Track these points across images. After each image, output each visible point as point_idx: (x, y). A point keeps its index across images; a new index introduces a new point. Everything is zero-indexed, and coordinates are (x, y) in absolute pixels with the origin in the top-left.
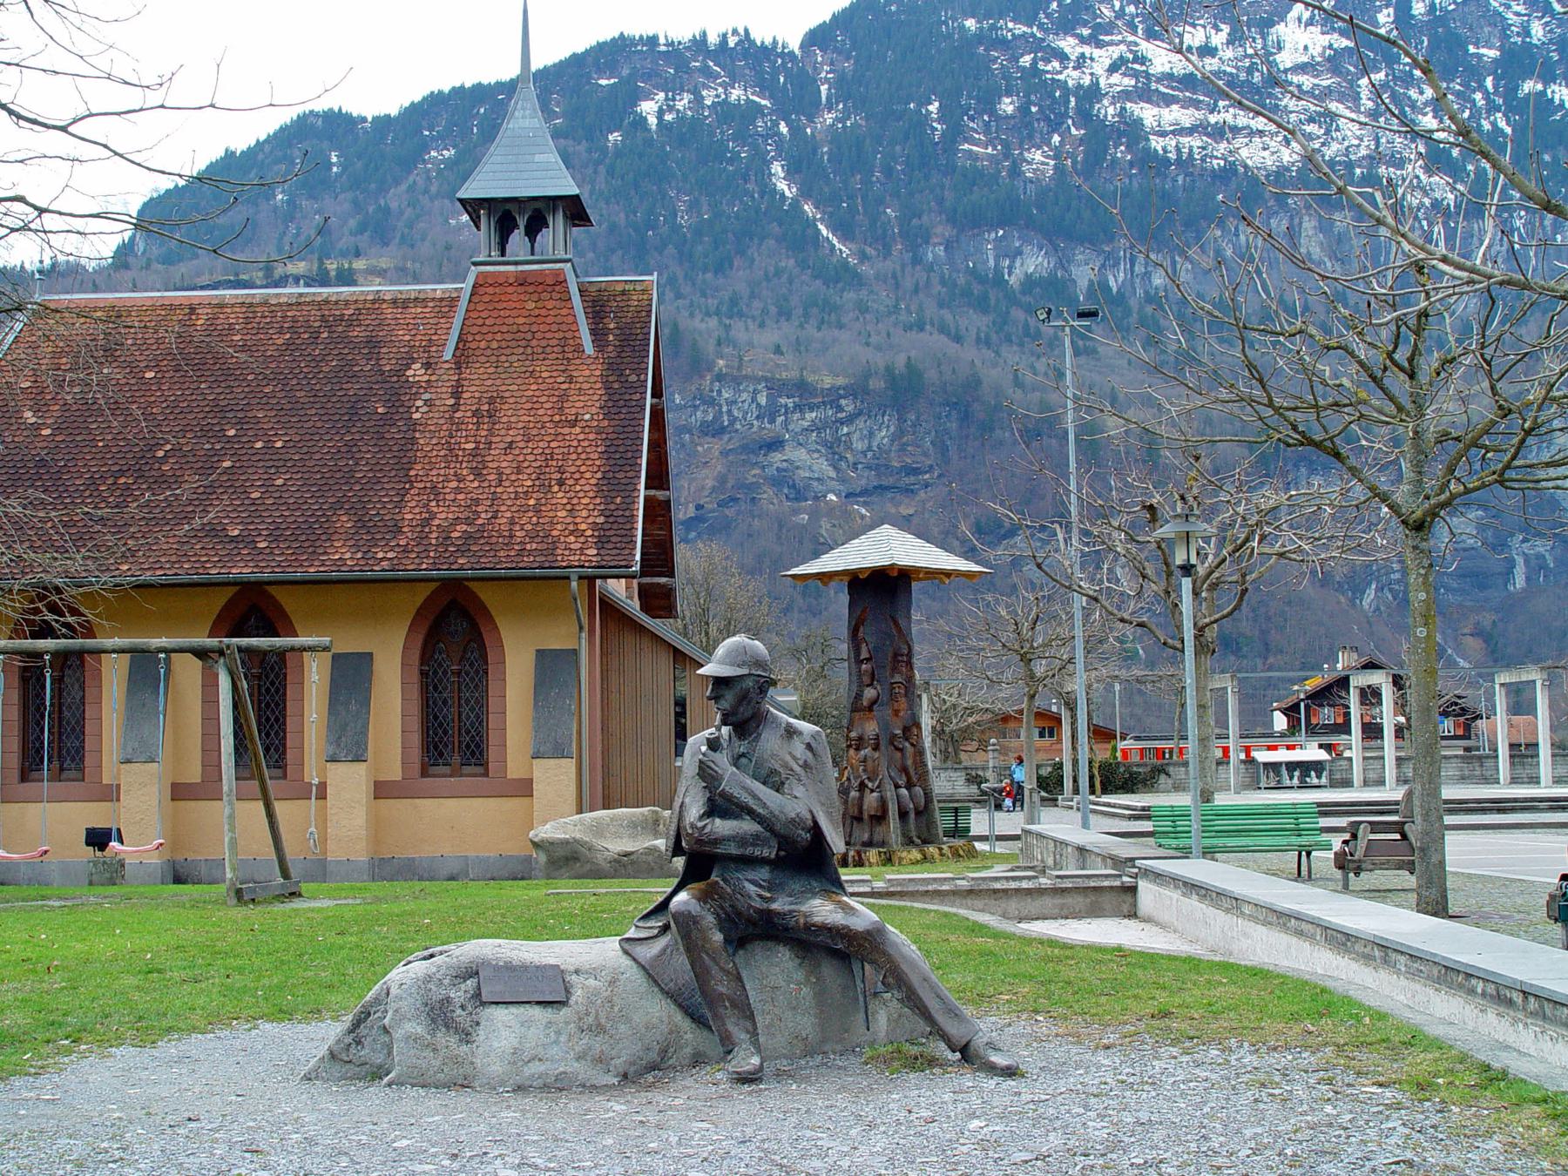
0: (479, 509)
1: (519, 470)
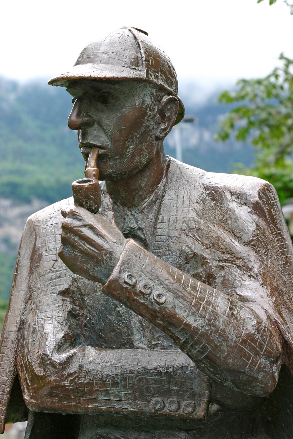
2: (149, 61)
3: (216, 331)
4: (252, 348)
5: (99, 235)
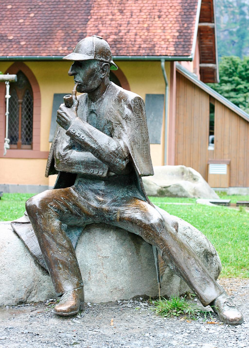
0: (122, 28)
1: (141, 11)
2: (96, 52)
3: (101, 149)
4: (114, 155)
5: (67, 116)
